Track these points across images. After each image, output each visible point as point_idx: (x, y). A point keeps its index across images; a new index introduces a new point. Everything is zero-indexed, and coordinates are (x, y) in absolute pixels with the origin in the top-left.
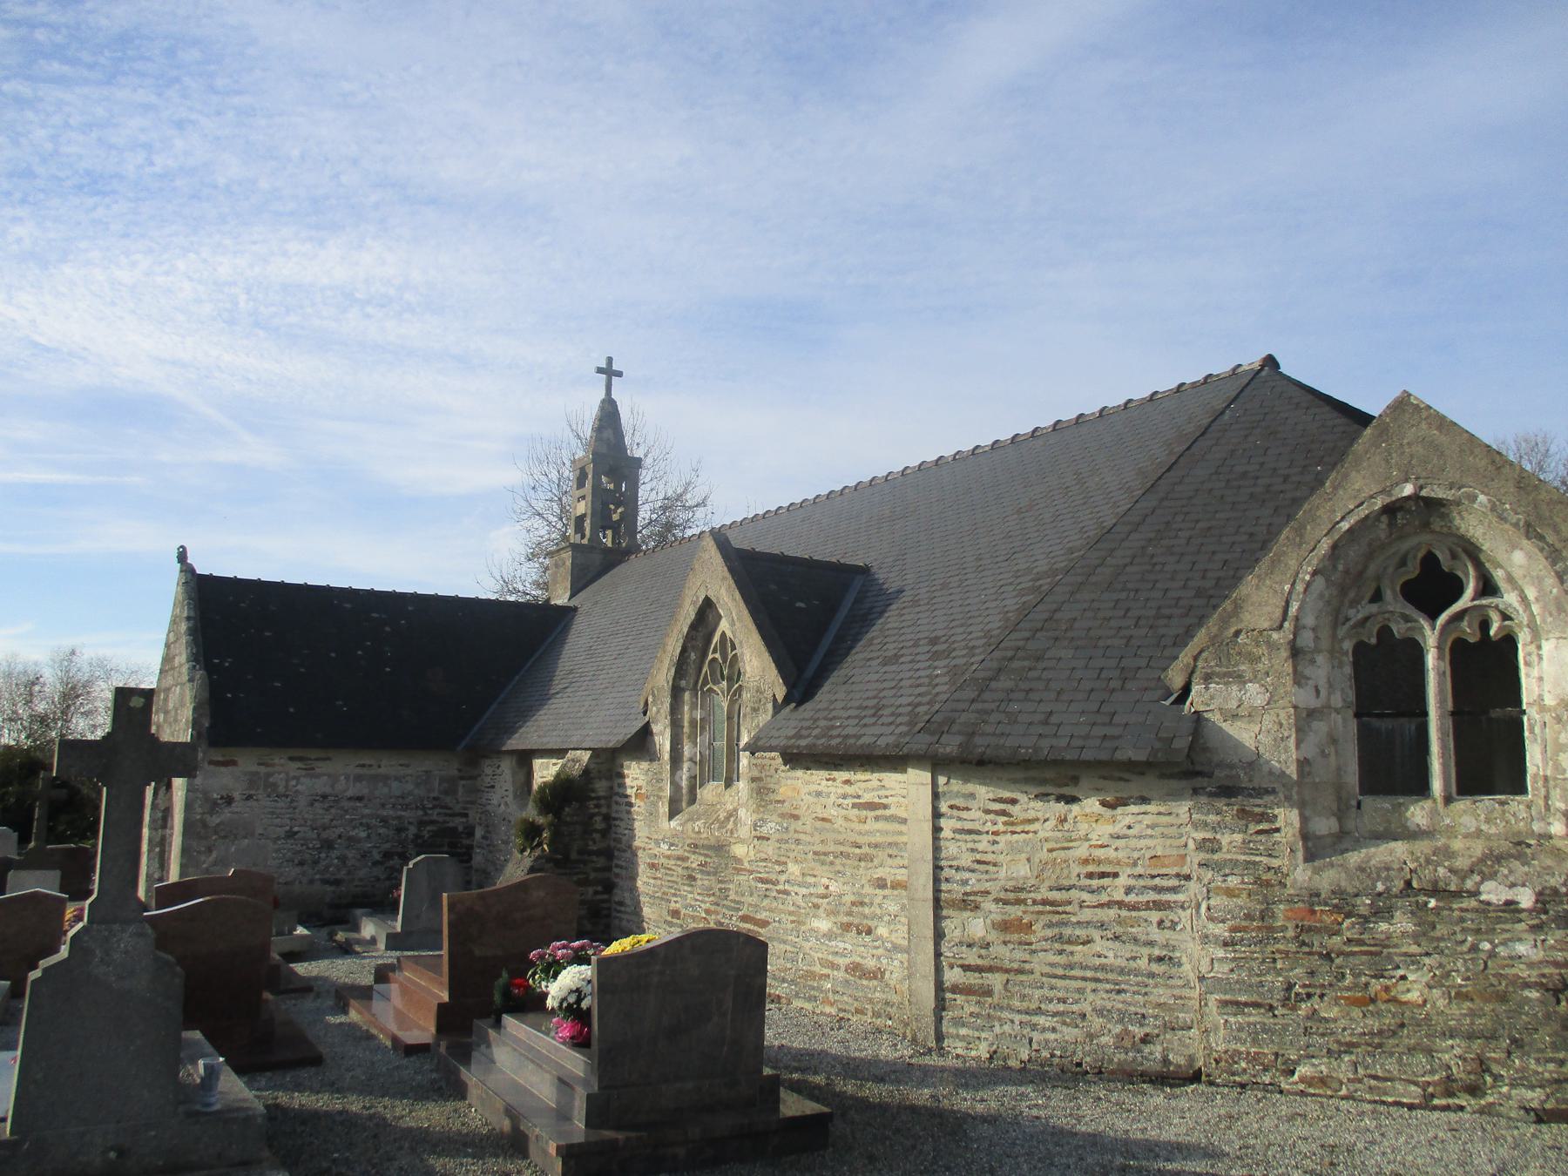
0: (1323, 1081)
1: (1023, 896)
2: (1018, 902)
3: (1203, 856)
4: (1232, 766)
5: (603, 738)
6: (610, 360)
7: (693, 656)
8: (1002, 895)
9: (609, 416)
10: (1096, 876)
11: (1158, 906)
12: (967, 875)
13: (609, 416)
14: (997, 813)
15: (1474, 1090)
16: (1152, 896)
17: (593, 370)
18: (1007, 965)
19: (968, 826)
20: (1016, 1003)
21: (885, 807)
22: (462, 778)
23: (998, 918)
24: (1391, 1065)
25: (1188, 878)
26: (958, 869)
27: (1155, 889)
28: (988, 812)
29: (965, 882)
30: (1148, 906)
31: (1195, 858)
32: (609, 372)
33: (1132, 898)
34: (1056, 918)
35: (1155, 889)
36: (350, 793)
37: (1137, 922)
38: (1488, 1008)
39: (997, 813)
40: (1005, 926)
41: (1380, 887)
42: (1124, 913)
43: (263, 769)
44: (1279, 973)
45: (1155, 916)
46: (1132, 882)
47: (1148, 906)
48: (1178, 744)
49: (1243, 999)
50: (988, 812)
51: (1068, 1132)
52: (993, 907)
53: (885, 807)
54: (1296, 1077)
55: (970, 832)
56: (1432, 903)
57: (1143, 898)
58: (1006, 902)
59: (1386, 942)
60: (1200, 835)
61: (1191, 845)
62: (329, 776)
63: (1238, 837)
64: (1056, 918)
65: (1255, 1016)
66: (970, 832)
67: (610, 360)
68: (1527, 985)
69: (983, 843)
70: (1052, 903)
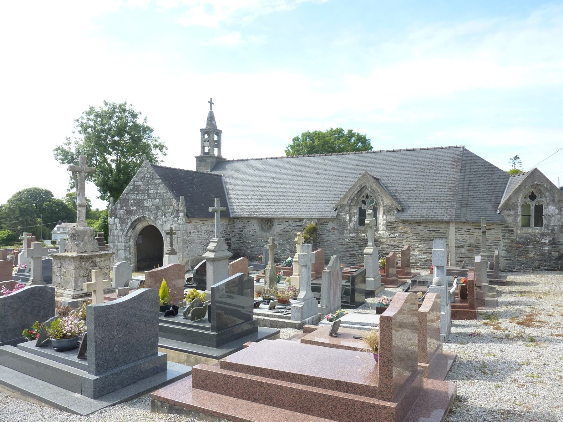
0: (519, 269)
1: (472, 245)
2: (471, 246)
3: (503, 237)
4: (508, 223)
5: (321, 216)
6: (211, 99)
7: (356, 198)
8: (468, 245)
9: (211, 118)
10: (85, 257)
11: (495, 245)
12: (461, 242)
13: (211, 118)
14: (467, 231)
15: (539, 268)
16: (495, 244)
17: (350, 129)
18: (469, 257)
19: (461, 234)
20: (470, 263)
21: (439, 231)
22: (229, 225)
23: (467, 249)
24: (528, 266)
25: (500, 241)
26: (460, 241)
27: (495, 243)
28: (465, 231)
29: (461, 243)
30: (493, 246)
31: (501, 238)
32: (211, 103)
33: (491, 244)
34: (477, 248)
35: (495, 243)
36: (211, 230)
37: (491, 248)
38: (541, 257)
39: (467, 231)
40: (469, 250)
41: (528, 241)
42: (490, 247)
43: (196, 224)
44: (513, 254)
45: (495, 247)
46: (491, 242)
47: (493, 246)
48: (335, 216)
49: (508, 258)
50: (465, 231)
51: (235, 316)
52: (466, 247)
53: (439, 231)
54: (515, 269)
55: (462, 235)
56: (535, 243)
57: (493, 244)
58: (468, 246)
59: (529, 248)
60: (503, 234)
61: (501, 236)
62: (207, 225)
63: (509, 234)
64: (477, 248)
65: (509, 261)
66: (462, 235)
67: (211, 99)
68: (547, 253)
69: (464, 236)
70: (477, 246)
